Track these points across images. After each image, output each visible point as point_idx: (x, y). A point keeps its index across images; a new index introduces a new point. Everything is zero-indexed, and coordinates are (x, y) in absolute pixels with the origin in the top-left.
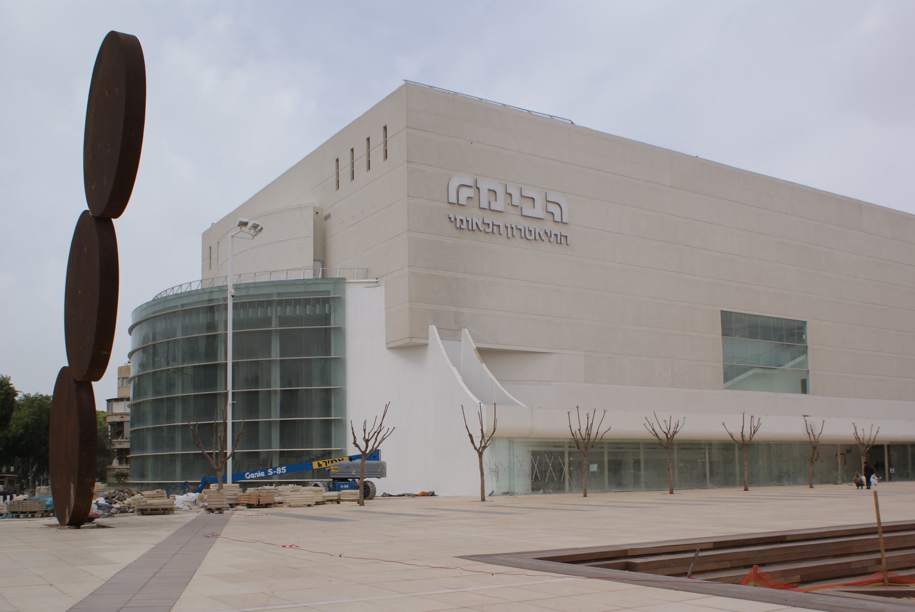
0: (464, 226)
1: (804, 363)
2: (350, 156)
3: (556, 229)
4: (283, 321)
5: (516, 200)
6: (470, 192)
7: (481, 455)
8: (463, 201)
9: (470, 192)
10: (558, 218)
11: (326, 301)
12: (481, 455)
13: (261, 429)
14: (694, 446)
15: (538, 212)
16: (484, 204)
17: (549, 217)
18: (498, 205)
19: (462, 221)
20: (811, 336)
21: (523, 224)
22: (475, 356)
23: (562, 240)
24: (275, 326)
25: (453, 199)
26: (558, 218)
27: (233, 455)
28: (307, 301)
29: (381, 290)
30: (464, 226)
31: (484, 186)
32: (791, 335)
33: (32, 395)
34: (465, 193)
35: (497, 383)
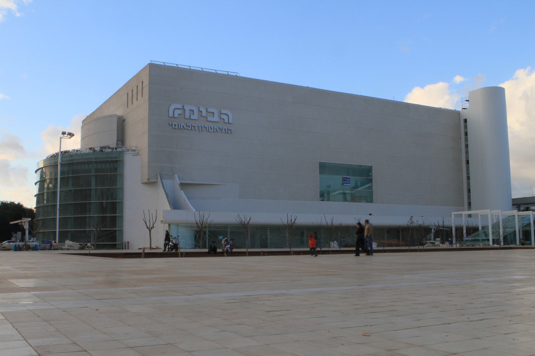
0: (177, 127)
1: (371, 188)
2: (129, 92)
3: (226, 127)
4: (96, 171)
5: (204, 113)
6: (180, 112)
7: (150, 231)
8: (176, 115)
9: (180, 112)
10: (226, 121)
11: (116, 161)
12: (150, 231)
13: (87, 220)
14: (263, 228)
15: (216, 119)
16: (187, 116)
17: (222, 121)
18: (195, 116)
19: (175, 125)
20: (375, 174)
21: (207, 125)
22: (178, 187)
23: (228, 131)
24: (93, 173)
25: (171, 114)
26: (226, 121)
27: (290, 248)
28: (107, 162)
29: (506, 86)
30: (177, 127)
31: (187, 108)
32: (365, 174)
33: (16, 203)
34: (177, 112)
35: (186, 199)
